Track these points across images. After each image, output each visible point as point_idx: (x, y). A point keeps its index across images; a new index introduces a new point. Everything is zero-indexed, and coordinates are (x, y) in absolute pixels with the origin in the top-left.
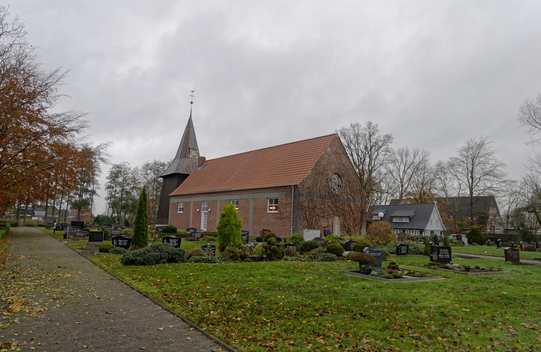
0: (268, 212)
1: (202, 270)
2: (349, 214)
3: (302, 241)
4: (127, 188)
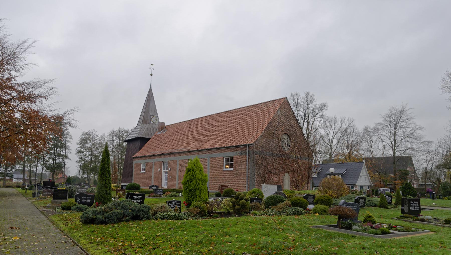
0: (224, 169)
1: (170, 229)
2: (298, 171)
4: (96, 152)
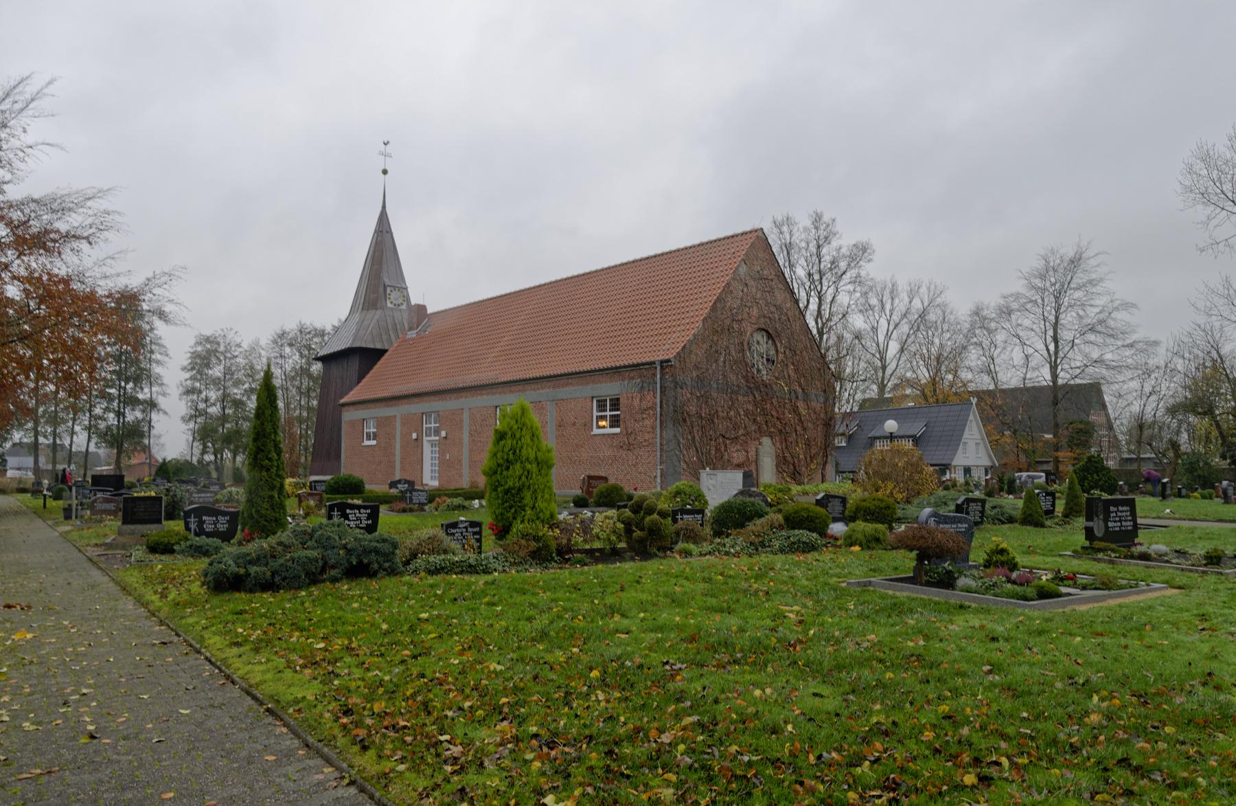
0: (596, 431)
1: (455, 599)
3: (700, 501)
4: (235, 391)
